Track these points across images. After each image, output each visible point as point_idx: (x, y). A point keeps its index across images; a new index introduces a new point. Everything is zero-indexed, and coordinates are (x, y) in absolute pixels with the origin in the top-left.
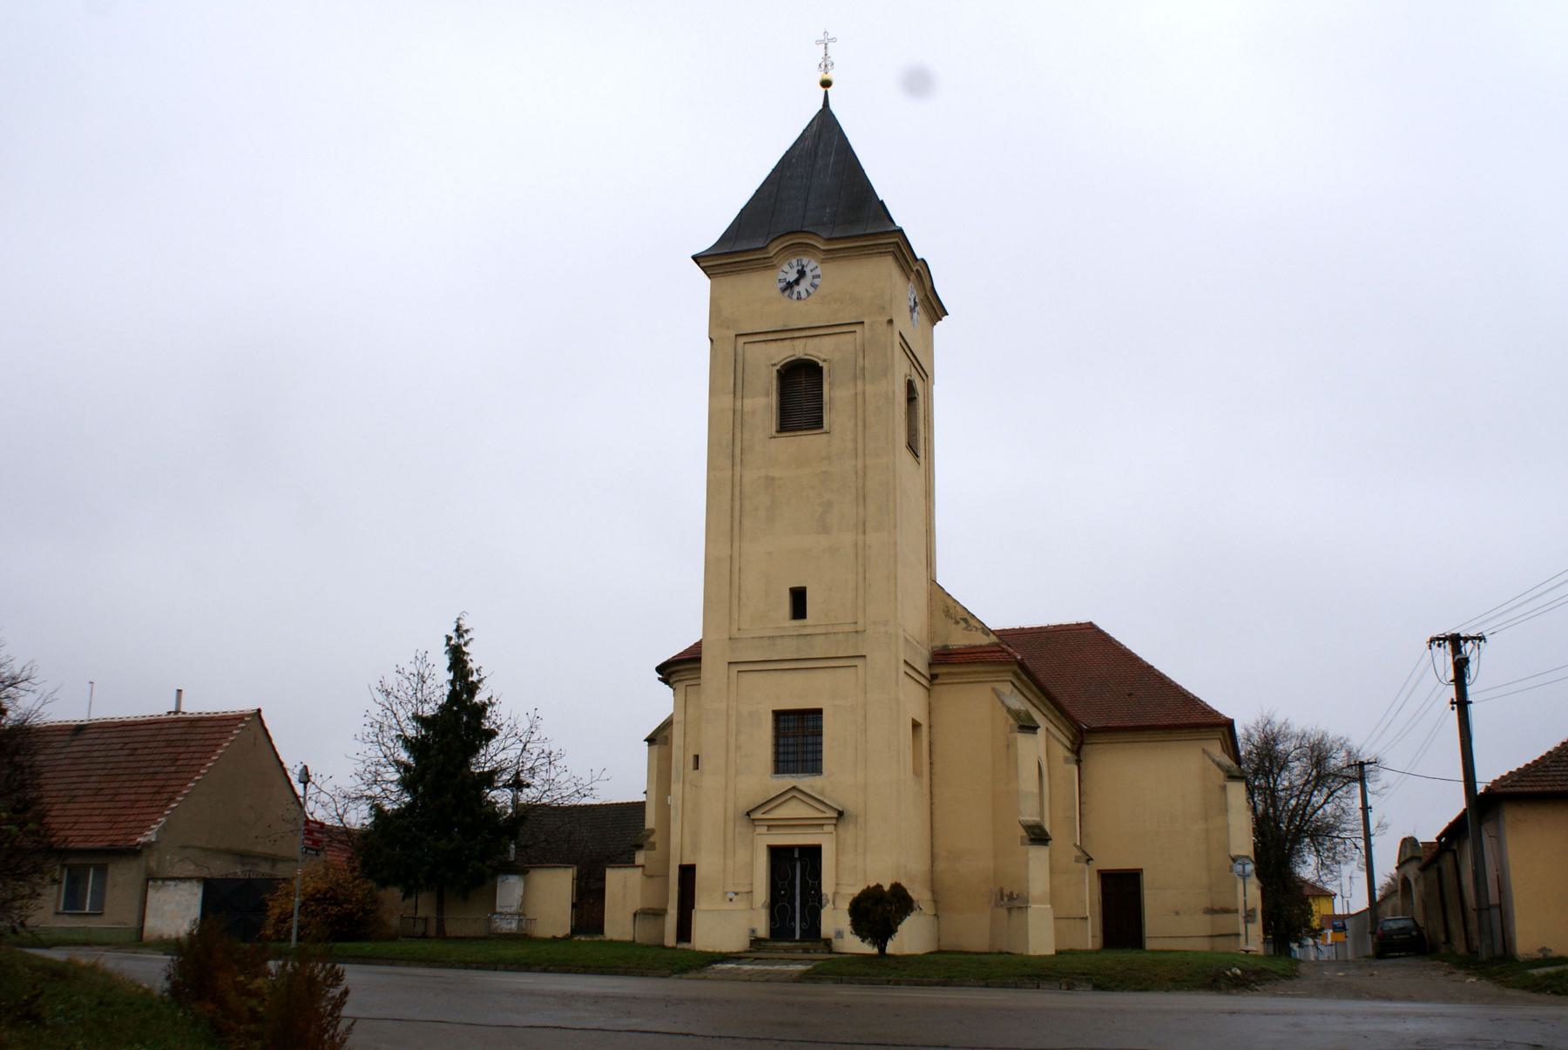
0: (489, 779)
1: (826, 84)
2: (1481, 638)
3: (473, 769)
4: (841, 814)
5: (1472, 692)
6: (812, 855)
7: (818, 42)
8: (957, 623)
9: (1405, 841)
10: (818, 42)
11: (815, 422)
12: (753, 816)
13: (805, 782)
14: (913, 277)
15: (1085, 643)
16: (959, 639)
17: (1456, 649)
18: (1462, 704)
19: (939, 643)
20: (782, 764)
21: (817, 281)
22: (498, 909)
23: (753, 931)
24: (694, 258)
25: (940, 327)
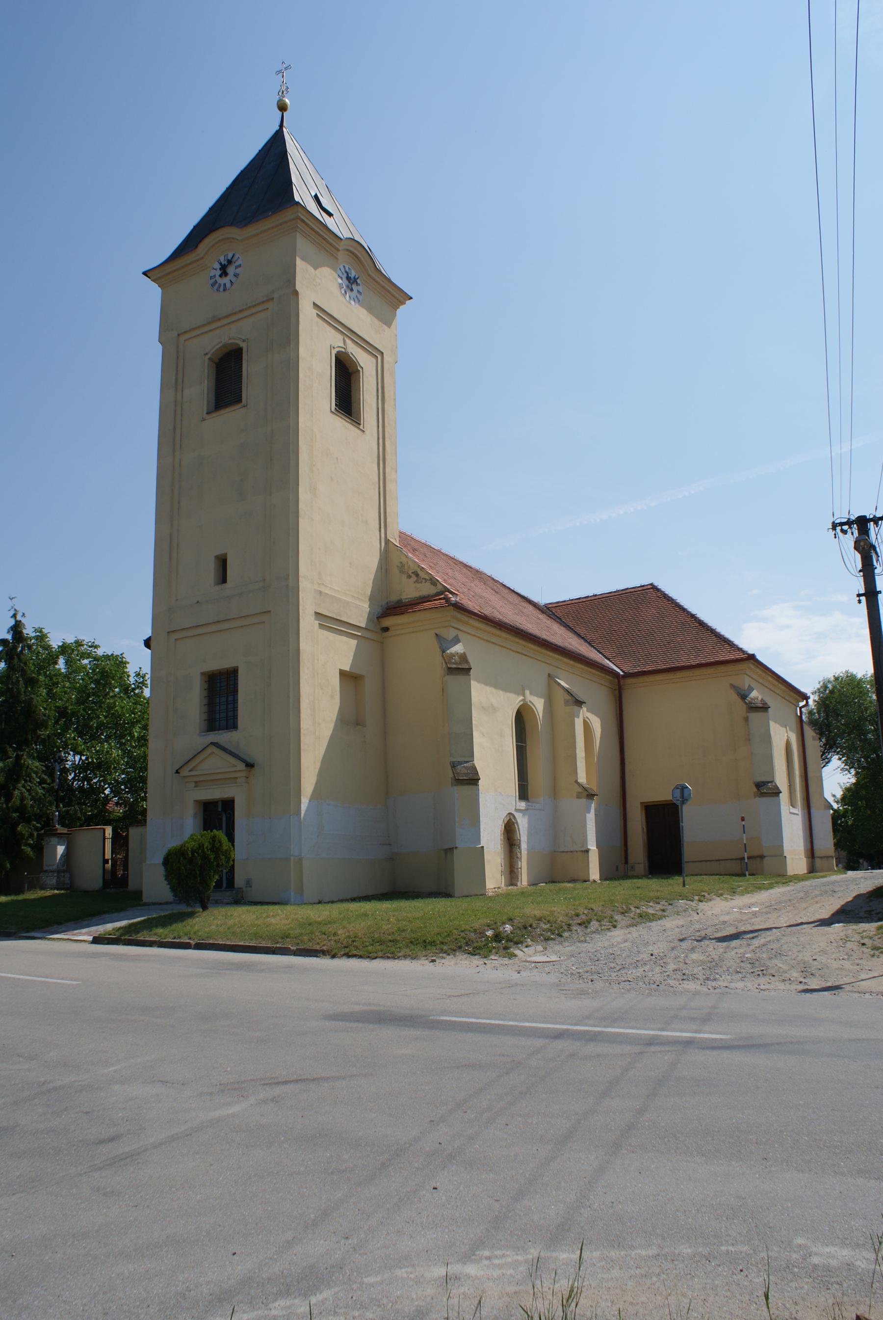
0: (863, 768)
1: (282, 108)
4: (250, 766)
5: (881, 583)
6: (228, 805)
8: (409, 577)
11: (237, 399)
13: (224, 737)
14: (342, 255)
16: (410, 591)
19: (394, 598)
22: (45, 868)
24: (145, 273)
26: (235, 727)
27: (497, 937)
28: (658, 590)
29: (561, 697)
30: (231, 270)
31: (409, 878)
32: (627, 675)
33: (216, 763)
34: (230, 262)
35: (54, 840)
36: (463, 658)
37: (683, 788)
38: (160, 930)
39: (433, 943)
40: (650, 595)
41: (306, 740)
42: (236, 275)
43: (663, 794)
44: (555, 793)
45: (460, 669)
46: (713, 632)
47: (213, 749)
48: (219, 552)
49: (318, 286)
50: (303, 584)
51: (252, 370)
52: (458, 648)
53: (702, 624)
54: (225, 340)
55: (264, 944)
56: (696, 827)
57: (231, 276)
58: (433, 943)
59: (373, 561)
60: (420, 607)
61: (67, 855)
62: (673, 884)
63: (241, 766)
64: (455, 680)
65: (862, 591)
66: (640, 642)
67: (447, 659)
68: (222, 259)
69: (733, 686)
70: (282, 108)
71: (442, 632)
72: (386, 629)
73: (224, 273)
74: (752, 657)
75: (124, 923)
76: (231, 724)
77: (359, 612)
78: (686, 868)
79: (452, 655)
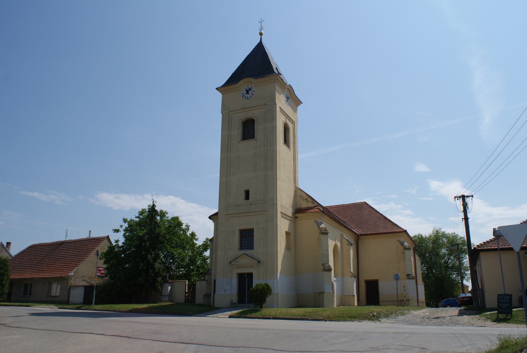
1: (261, 34)
2: (472, 196)
3: (120, 244)
4: (259, 262)
6: (250, 275)
7: (259, 22)
9: (177, 218)
10: (259, 22)
12: (232, 263)
13: (248, 252)
14: (286, 90)
15: (363, 209)
17: (464, 200)
18: (466, 219)
19: (298, 207)
20: (242, 247)
21: (253, 93)
23: (232, 301)
24: (217, 89)
25: (299, 107)
26: (253, 249)
27: (374, 316)
28: (368, 204)
29: (345, 242)
30: (250, 92)
31: (308, 301)
32: (361, 235)
33: (245, 260)
34: (250, 89)
35: (167, 284)
36: (325, 229)
37: (397, 275)
38: (254, 314)
39: (356, 317)
40: (364, 206)
41: (279, 254)
42: (252, 94)
43: (372, 277)
44: (343, 276)
45: (325, 233)
46: (390, 221)
47: (244, 256)
48: (246, 189)
49: (281, 101)
50: (278, 202)
51: (259, 128)
52: (323, 226)
53: (386, 218)
54: (248, 116)
55: (298, 317)
56: (385, 289)
57: (250, 94)
58: (356, 317)
59: (292, 194)
60: (308, 211)
61: (171, 290)
62: (374, 309)
63: (257, 262)
64: (323, 237)
65: (321, 168)
66: (361, 222)
67: (320, 229)
68: (247, 88)
69: (398, 241)
70: (261, 34)
71: (317, 220)
72: (296, 218)
73: (248, 93)
74: (406, 231)
75: (240, 311)
76: (251, 247)
77: (290, 212)
78: (381, 303)
79: (322, 228)
